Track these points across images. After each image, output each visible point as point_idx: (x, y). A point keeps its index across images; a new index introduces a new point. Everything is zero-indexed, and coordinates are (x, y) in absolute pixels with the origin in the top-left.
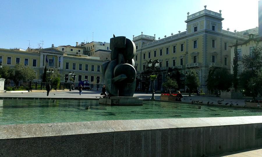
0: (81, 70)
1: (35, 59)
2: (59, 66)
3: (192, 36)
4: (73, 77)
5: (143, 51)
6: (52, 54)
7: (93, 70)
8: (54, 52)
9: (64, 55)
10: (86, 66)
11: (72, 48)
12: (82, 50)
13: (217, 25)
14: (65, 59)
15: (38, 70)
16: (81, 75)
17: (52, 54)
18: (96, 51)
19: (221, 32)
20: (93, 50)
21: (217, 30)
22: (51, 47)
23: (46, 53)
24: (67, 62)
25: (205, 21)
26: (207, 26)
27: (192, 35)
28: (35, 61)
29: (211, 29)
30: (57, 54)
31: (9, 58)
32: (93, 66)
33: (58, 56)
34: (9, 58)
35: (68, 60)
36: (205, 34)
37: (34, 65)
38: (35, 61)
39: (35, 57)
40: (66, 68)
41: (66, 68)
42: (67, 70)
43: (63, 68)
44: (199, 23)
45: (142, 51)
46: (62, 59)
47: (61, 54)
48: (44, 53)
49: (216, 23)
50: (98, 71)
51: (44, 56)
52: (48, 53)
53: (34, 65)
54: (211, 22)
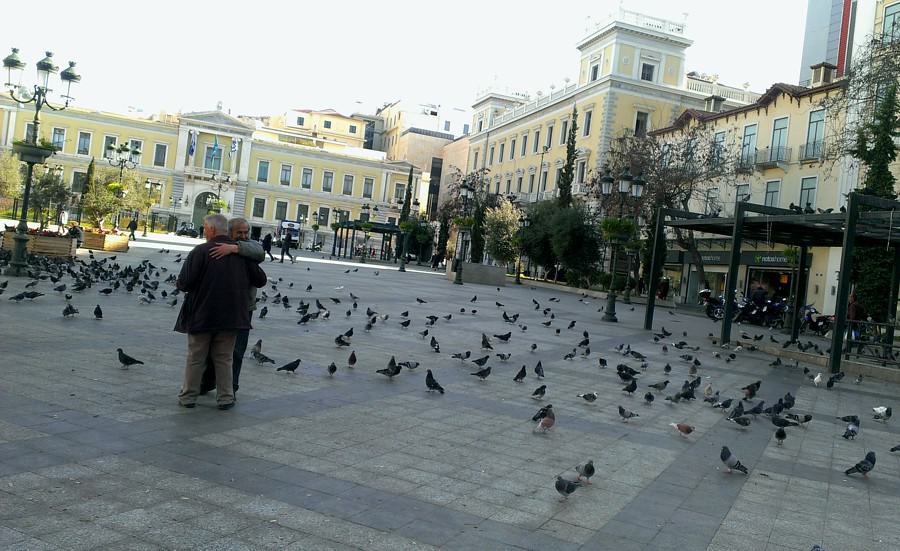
0: (308, 187)
1: (163, 143)
2: (237, 171)
3: (662, 96)
4: (148, 186)
5: (492, 138)
6: (216, 133)
7: (347, 192)
8: (224, 125)
9: (256, 136)
10: (345, 180)
11: (328, 119)
12: (361, 129)
13: (663, 64)
14: (256, 149)
15: (170, 178)
16: (263, 197)
17: (216, 133)
18: (404, 134)
19: (677, 85)
20: (397, 128)
21: (661, 79)
22: (374, 114)
23: (198, 126)
24: (265, 159)
25: (614, 46)
26: (623, 63)
27: (585, 92)
28: (161, 150)
29: (636, 72)
30: (231, 132)
31: (85, 136)
32: (349, 180)
33: (237, 137)
34: (85, 136)
35: (266, 154)
36: (608, 89)
37: (159, 162)
38: (161, 150)
39: (163, 138)
40: (260, 179)
41: (260, 179)
42: (305, 189)
43: (250, 178)
44: (603, 53)
45: (490, 138)
46: (246, 147)
47: (244, 134)
48: (192, 128)
49: (660, 53)
50: (365, 196)
51: (190, 135)
52: (205, 127)
53: (159, 162)
54: (637, 52)
